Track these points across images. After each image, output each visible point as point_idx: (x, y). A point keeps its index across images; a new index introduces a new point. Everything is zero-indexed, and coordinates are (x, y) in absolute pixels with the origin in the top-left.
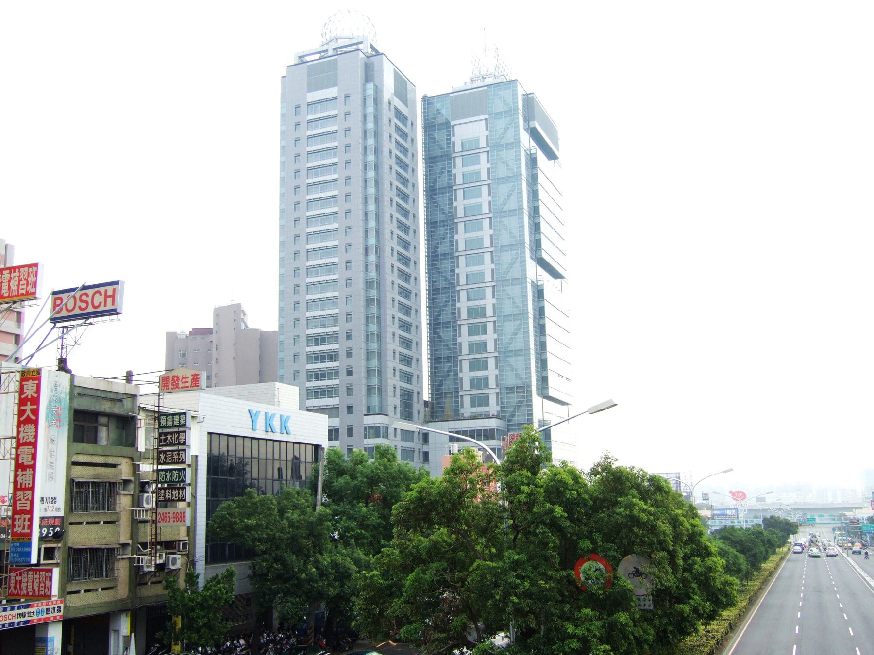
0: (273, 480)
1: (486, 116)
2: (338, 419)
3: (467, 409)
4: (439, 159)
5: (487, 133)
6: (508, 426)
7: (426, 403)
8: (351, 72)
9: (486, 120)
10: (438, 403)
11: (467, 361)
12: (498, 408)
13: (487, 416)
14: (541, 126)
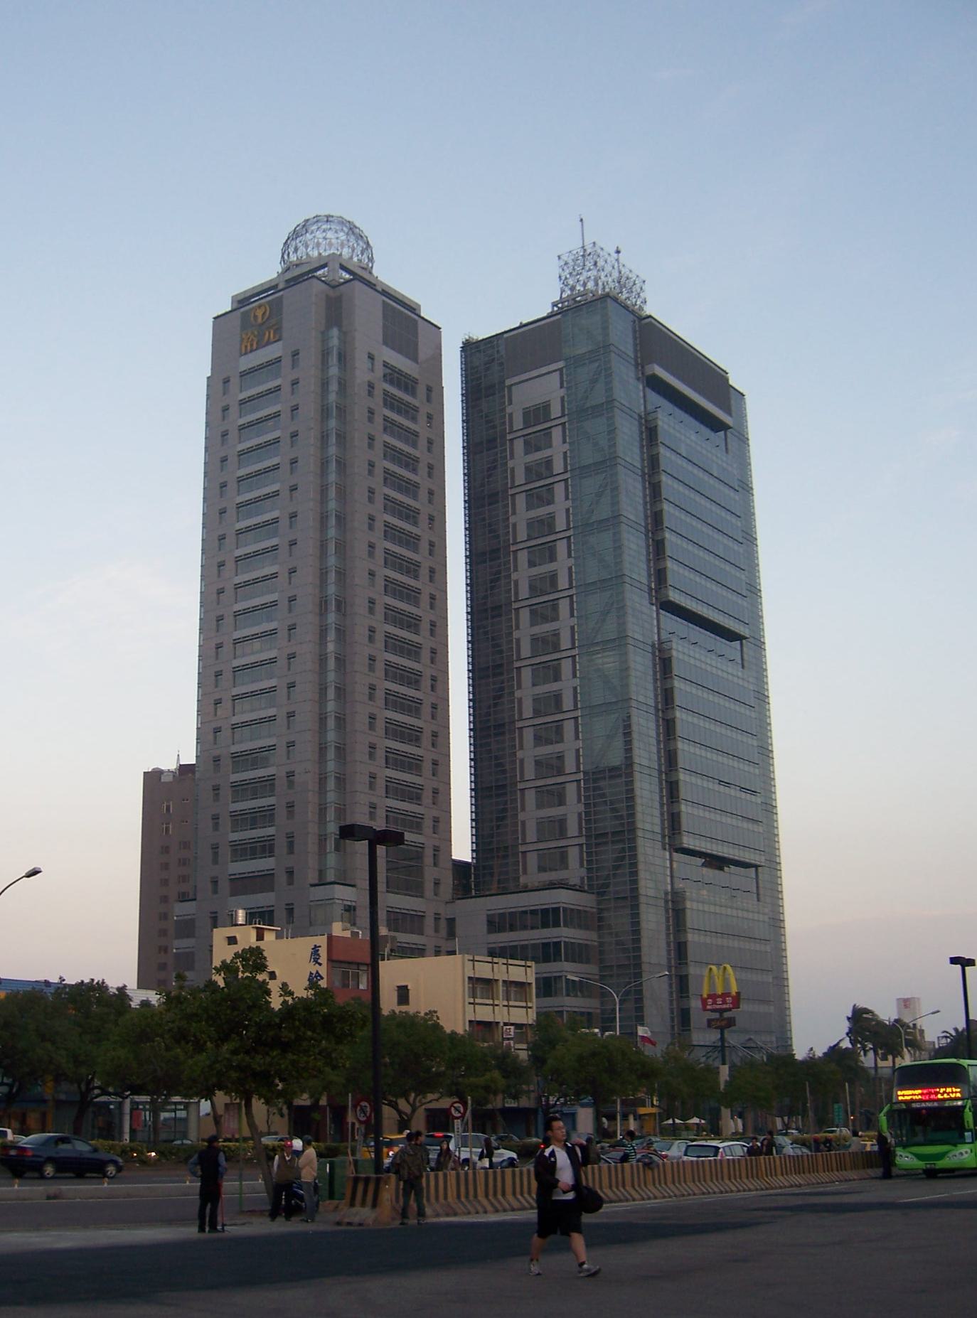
0: (547, 986)
1: (561, 364)
2: (272, 895)
3: (532, 876)
4: (731, 636)
5: (562, 392)
6: (599, 903)
7: (460, 866)
8: (304, 315)
9: (561, 370)
10: (484, 868)
11: (533, 791)
12: (583, 872)
13: (562, 885)
14: (667, 369)
